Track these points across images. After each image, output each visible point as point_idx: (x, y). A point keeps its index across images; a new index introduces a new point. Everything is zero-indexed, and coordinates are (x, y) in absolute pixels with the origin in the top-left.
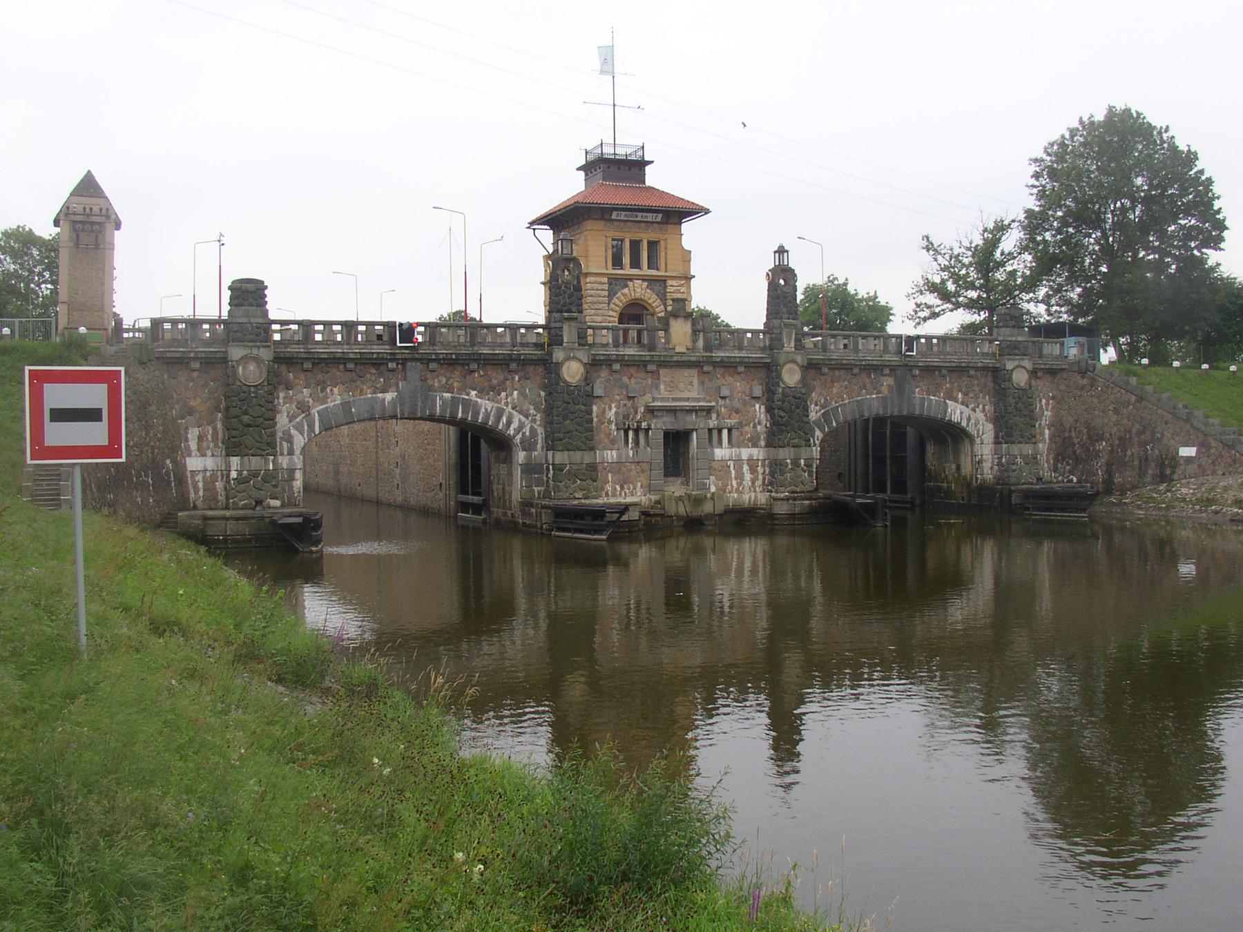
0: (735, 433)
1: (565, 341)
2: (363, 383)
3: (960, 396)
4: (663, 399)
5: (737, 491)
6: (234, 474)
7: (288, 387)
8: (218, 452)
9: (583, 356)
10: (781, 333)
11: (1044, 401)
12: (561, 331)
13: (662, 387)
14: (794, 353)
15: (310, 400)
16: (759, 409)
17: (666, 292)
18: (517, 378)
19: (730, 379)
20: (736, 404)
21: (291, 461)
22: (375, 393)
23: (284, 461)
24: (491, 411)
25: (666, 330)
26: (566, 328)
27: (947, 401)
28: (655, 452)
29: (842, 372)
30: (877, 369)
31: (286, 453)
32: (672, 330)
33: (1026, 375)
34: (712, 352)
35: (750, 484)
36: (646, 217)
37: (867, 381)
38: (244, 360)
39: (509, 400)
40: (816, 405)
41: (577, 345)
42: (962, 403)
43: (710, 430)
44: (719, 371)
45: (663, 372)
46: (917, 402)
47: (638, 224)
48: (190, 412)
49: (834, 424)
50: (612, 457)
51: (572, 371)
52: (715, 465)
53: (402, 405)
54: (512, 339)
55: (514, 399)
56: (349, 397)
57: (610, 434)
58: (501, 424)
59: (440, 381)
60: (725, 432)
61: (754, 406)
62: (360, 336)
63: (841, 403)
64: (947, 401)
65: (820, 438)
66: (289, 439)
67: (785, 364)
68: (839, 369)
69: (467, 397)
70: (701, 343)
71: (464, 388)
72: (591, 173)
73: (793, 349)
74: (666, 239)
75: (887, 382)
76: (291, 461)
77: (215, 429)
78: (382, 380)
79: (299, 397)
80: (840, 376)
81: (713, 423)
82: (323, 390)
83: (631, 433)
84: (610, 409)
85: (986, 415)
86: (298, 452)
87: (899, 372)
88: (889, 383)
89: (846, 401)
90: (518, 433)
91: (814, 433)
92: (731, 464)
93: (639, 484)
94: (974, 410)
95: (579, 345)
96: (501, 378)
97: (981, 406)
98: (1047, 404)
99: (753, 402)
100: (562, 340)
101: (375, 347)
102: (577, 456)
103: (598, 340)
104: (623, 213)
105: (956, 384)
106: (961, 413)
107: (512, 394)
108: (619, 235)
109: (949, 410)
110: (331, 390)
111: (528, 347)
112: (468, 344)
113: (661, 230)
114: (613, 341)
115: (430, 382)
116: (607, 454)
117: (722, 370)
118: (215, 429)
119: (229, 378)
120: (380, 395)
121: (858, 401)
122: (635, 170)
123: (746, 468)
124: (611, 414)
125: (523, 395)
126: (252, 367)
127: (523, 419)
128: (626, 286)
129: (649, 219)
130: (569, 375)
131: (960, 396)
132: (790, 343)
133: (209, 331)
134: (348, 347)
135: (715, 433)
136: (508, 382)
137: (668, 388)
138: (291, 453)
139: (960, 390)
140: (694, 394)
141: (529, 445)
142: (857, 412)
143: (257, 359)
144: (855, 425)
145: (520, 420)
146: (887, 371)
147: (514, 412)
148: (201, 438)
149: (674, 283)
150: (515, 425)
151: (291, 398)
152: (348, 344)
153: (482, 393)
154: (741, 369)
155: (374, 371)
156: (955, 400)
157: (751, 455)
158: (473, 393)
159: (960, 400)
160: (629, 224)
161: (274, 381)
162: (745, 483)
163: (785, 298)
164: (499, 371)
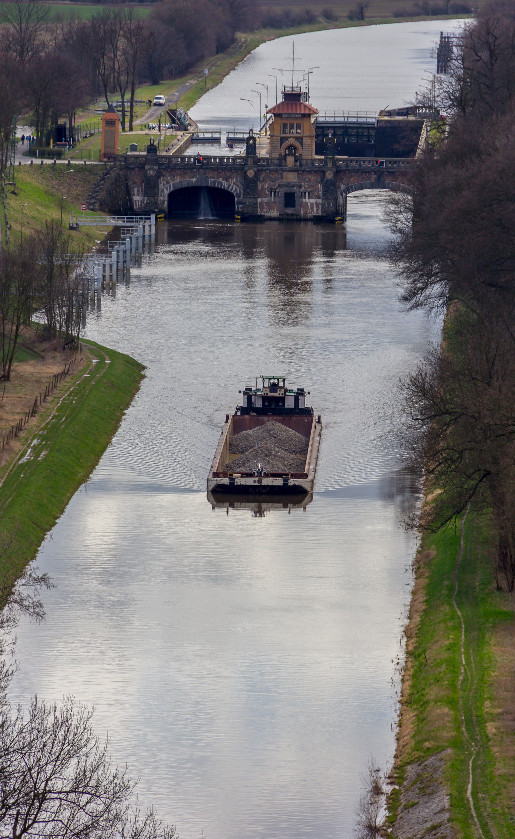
0: (311, 194)
5: (311, 213)
6: (145, 202)
7: (164, 176)
8: (143, 195)
16: (320, 186)
25: (286, 161)
26: (249, 160)
28: (281, 200)
30: (369, 172)
32: (287, 160)
37: (365, 176)
38: (150, 169)
43: (301, 193)
45: (285, 173)
48: (135, 183)
51: (251, 173)
52: (303, 204)
53: (198, 182)
60: (307, 193)
66: (163, 191)
70: (298, 164)
71: (218, 177)
77: (142, 188)
81: (302, 190)
82: (174, 177)
92: (309, 204)
96: (230, 174)
102: (251, 200)
118: (142, 188)
119: (145, 174)
123: (315, 205)
124: (266, 187)
125: (237, 179)
135: (303, 194)
141: (239, 196)
143: (153, 169)
144: (144, 240)
148: (138, 191)
149: (306, 139)
150: (234, 189)
154: (313, 172)
158: (221, 179)
161: (159, 175)
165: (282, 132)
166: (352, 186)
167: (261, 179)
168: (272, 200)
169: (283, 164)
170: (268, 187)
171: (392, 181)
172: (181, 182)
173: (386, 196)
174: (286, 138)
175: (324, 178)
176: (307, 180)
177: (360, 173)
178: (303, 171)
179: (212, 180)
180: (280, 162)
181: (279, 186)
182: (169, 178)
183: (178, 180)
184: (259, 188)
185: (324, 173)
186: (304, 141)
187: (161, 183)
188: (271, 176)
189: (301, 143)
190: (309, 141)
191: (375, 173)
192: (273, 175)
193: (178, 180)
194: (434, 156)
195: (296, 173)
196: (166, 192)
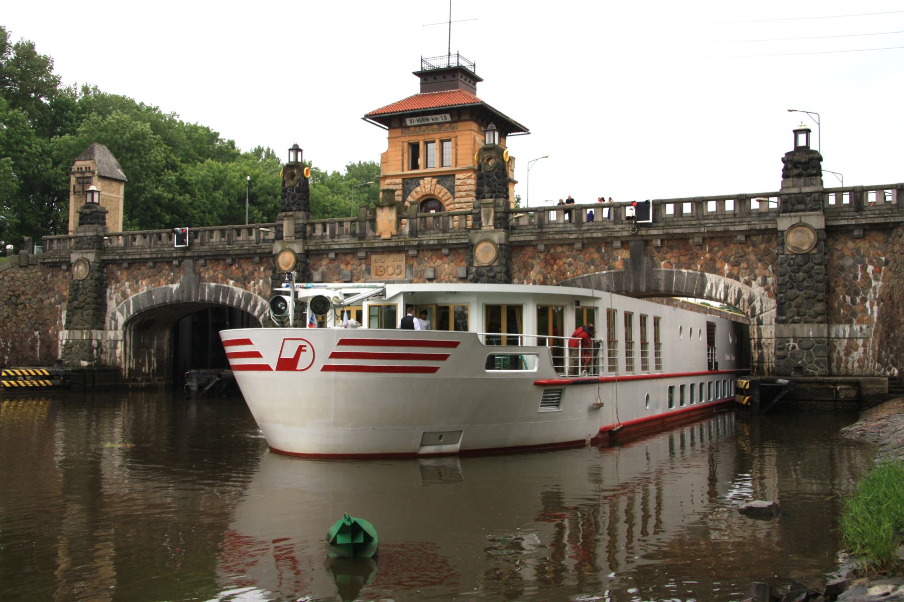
1: (284, 235)
2: (160, 277)
3: (726, 267)
9: (298, 248)
11: (870, 268)
12: (282, 227)
14: (493, 232)
17: (403, 184)
18: (262, 269)
19: (439, 262)
23: (111, 334)
27: (707, 274)
29: (565, 249)
30: (607, 241)
31: (113, 328)
32: (379, 219)
33: (812, 236)
36: (436, 119)
37: (596, 256)
38: (78, 261)
39: (256, 287)
41: (293, 238)
42: (730, 276)
45: (374, 257)
46: (662, 277)
54: (257, 237)
55: (259, 287)
58: (249, 307)
59: (209, 274)
60: (113, 328)
64: (707, 274)
66: (114, 318)
68: (562, 245)
69: (226, 286)
70: (406, 229)
71: (225, 279)
73: (493, 228)
74: (456, 137)
75: (624, 255)
76: (116, 334)
78: (172, 274)
79: (123, 288)
82: (137, 283)
85: (767, 289)
86: (120, 327)
88: (623, 257)
90: (261, 315)
96: (251, 269)
97: (759, 279)
100: (283, 235)
104: (415, 119)
108: (413, 139)
111: (268, 242)
113: (452, 128)
117: (430, 253)
120: (170, 286)
121: (582, 278)
128: (419, 185)
129: (440, 120)
130: (283, 265)
138: (116, 329)
145: (262, 304)
153: (237, 281)
155: (76, 268)
158: (231, 282)
159: (727, 272)
169: (370, 233)
171: (679, 265)
172: (149, 293)
173: (228, 485)
174: (416, 180)
175: (471, 264)
177: (125, 265)
178: (420, 248)
179: (213, 284)
180: (363, 228)
182: (127, 284)
186: (457, 182)
188: (342, 266)
189: (452, 190)
190: (469, 181)
191: (625, 244)
193: (144, 287)
195: (402, 257)
196: (121, 320)
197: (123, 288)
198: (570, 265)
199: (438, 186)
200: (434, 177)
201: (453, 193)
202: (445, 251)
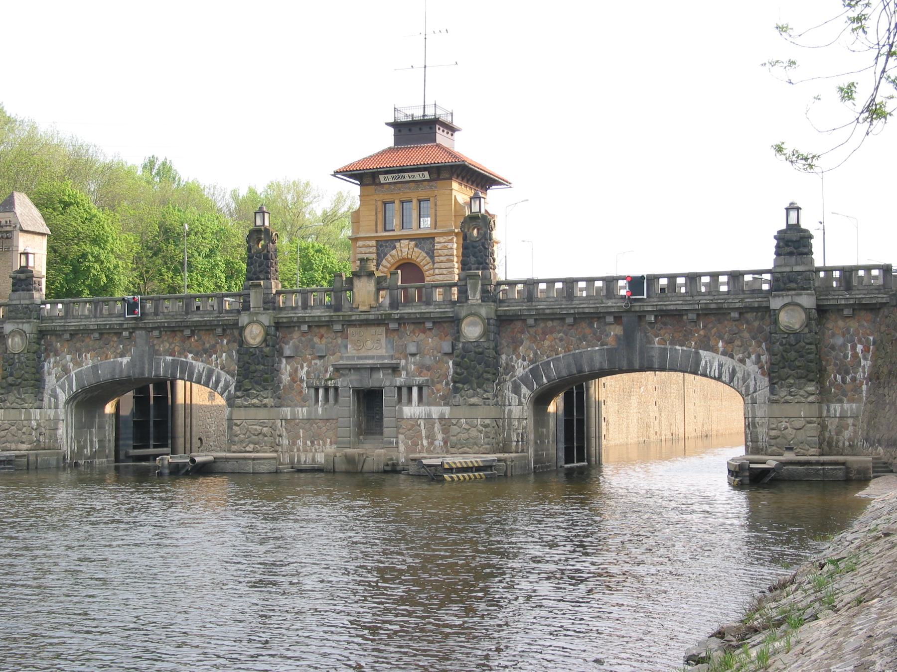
0: (425, 390)
3: (720, 344)
4: (348, 358)
7: (56, 354)
10: (466, 285)
11: (859, 348)
13: (349, 346)
14: (480, 305)
15: (72, 365)
18: (225, 341)
19: (422, 336)
20: (428, 361)
21: (56, 413)
22: (116, 358)
24: (203, 372)
27: (701, 351)
29: (556, 323)
31: (53, 407)
34: (398, 309)
35: (442, 444)
36: (414, 176)
37: (587, 330)
38: (13, 333)
40: (524, 360)
42: (724, 353)
44: (410, 328)
45: (351, 330)
47: (408, 185)
49: (545, 380)
50: (303, 414)
51: (254, 335)
56: (98, 360)
57: (301, 392)
59: (164, 346)
60: (415, 391)
61: (448, 363)
62: (834, 283)
63: (554, 357)
64: (701, 351)
65: (527, 396)
67: (465, 317)
68: (552, 320)
71: (183, 352)
72: (443, 131)
73: (480, 301)
75: (616, 331)
78: (121, 346)
80: (553, 327)
81: (400, 380)
82: (80, 356)
83: (321, 392)
84: (302, 368)
85: (761, 368)
86: (61, 405)
87: (625, 319)
89: (561, 355)
90: (225, 391)
91: (520, 391)
93: (329, 441)
94: (742, 361)
95: (264, 309)
97: (753, 357)
98: (866, 350)
99: (445, 358)
101: (114, 319)
103: (288, 304)
104: (390, 176)
105: (714, 330)
106: (721, 366)
107: (221, 357)
108: (387, 198)
109: (703, 363)
110: (86, 356)
112: (184, 313)
113: (431, 187)
114: (302, 303)
115: (157, 347)
116: (298, 411)
117: (412, 327)
120: (119, 359)
122: (426, 129)
123: (437, 427)
124: (303, 373)
125: (230, 356)
126: (17, 339)
127: (229, 377)
129: (418, 178)
131: (720, 344)
132: (474, 295)
133: (586, 289)
134: (95, 320)
135: (405, 391)
136: (218, 345)
137: (356, 348)
139: (721, 337)
140: (383, 352)
142: (573, 366)
143: (22, 333)
145: (225, 380)
146: (610, 319)
147: (222, 372)
149: (441, 239)
151: (59, 363)
152: (95, 317)
153: (197, 356)
156: (714, 350)
157: (442, 414)
158: (190, 356)
159: (721, 349)
160: (399, 186)
162: (437, 443)
163: (474, 247)
164: (211, 336)
165: (380, 227)
166: (548, 363)
167: (287, 351)
168: (320, 410)
170: (308, 373)
171: (673, 343)
172: (95, 368)
174: (391, 242)
176: (412, 349)
179: (169, 358)
181: (337, 369)
182: (68, 357)
183: (89, 362)
184: (285, 378)
185: (456, 321)
186: (437, 246)
187: (49, 374)
189: (431, 254)
191: (618, 319)
192: (322, 337)
193: (89, 362)
194: (686, 285)
196: (63, 397)
197: (64, 361)
198: (561, 340)
199: (416, 249)
200: (411, 240)
201: (432, 257)
202: (429, 325)
